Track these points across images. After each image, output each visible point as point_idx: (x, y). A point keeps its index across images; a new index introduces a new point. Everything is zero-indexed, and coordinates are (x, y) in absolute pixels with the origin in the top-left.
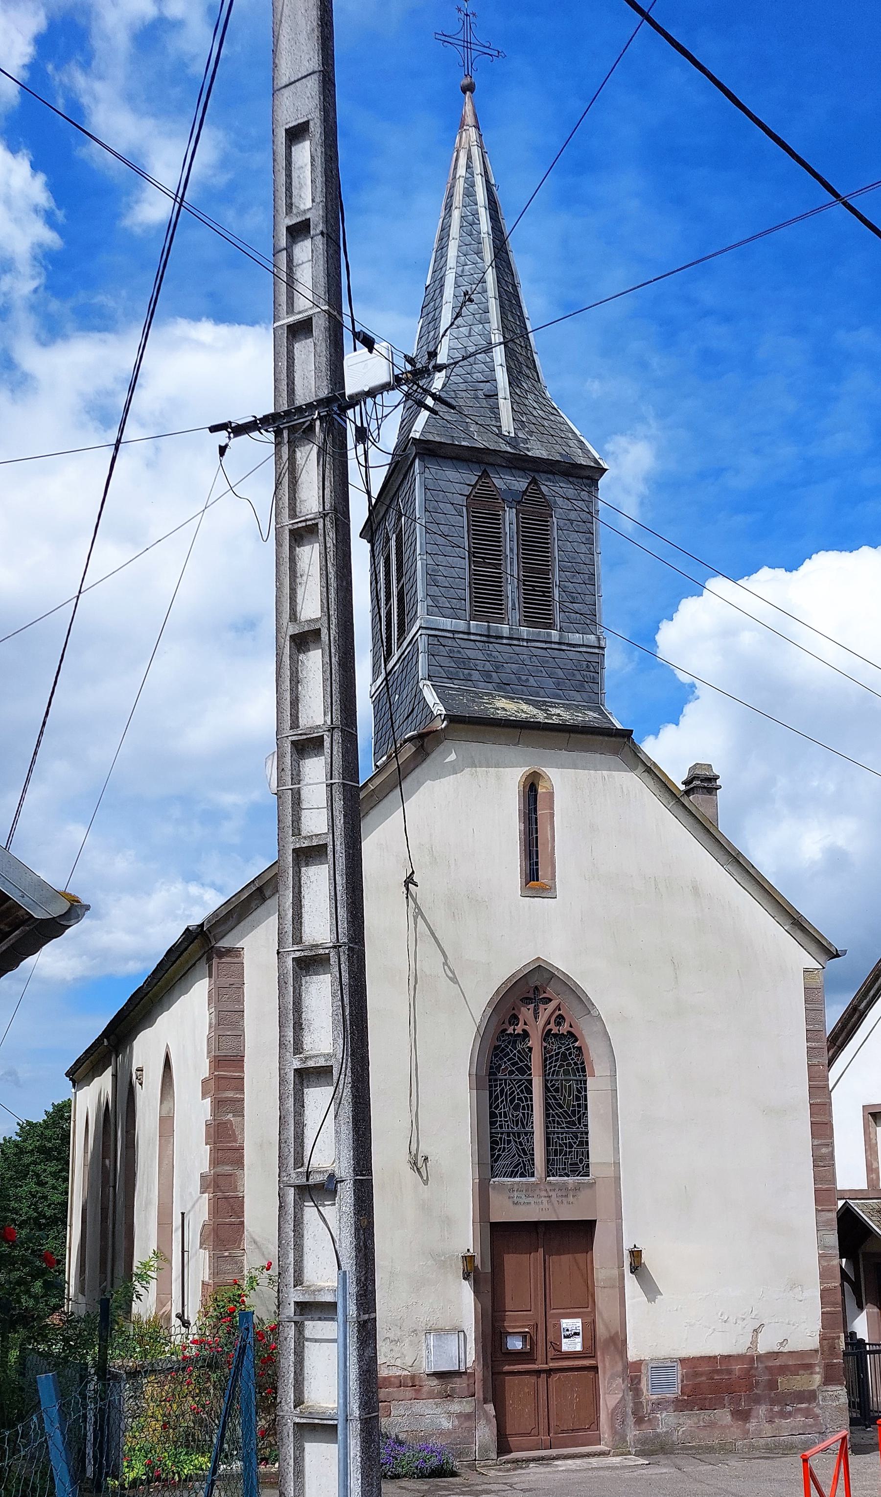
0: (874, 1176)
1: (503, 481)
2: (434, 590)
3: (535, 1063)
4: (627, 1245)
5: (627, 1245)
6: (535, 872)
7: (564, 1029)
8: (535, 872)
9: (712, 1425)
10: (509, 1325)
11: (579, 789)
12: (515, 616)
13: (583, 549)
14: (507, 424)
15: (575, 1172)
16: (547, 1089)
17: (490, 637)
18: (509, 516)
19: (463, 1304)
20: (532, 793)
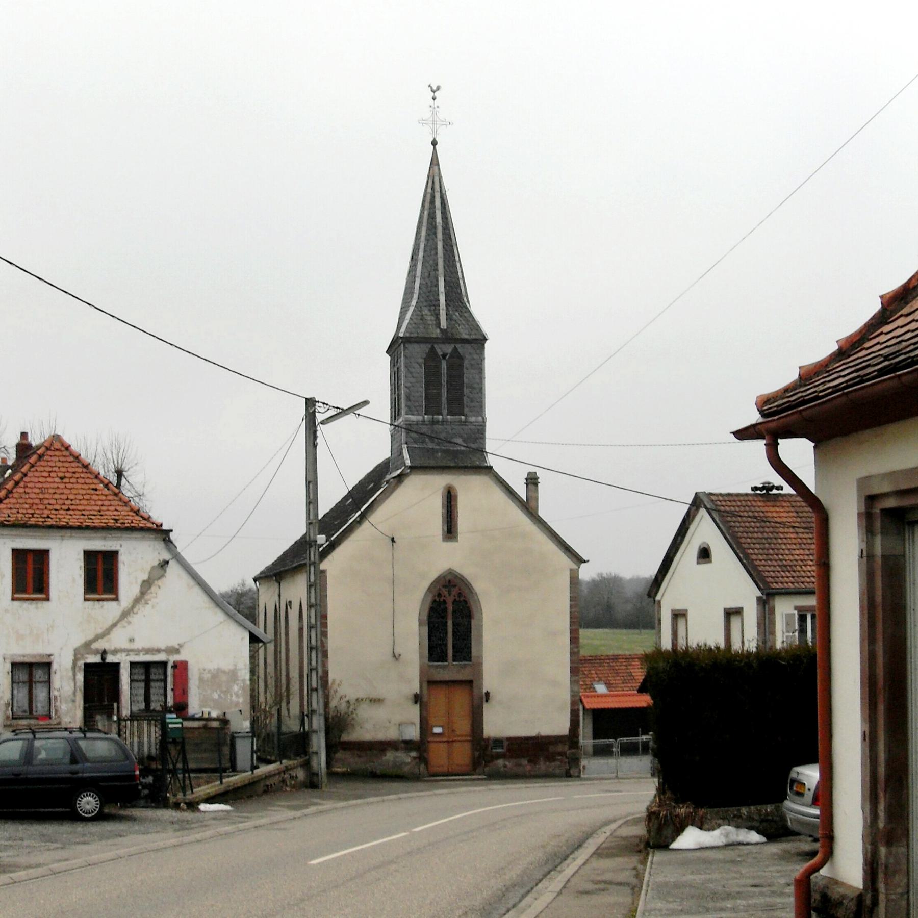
0: (88, 803)
1: (440, 349)
2: (409, 403)
3: (450, 618)
4: (750, 492)
5: (484, 691)
6: (450, 531)
7: (462, 599)
8: (450, 531)
9: (520, 765)
10: (432, 721)
11: (472, 492)
12: (445, 411)
13: (477, 377)
14: (444, 324)
15: (465, 660)
16: (454, 625)
17: (434, 422)
18: (444, 365)
19: (414, 713)
20: (450, 499)
